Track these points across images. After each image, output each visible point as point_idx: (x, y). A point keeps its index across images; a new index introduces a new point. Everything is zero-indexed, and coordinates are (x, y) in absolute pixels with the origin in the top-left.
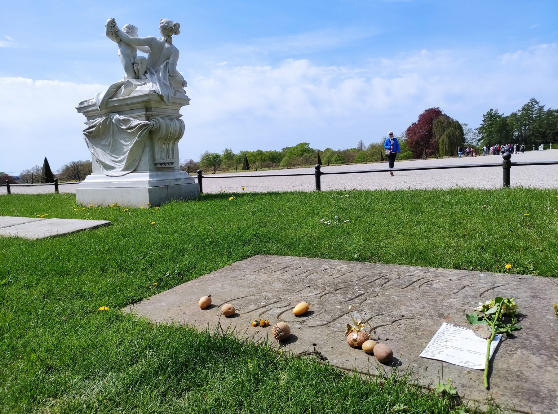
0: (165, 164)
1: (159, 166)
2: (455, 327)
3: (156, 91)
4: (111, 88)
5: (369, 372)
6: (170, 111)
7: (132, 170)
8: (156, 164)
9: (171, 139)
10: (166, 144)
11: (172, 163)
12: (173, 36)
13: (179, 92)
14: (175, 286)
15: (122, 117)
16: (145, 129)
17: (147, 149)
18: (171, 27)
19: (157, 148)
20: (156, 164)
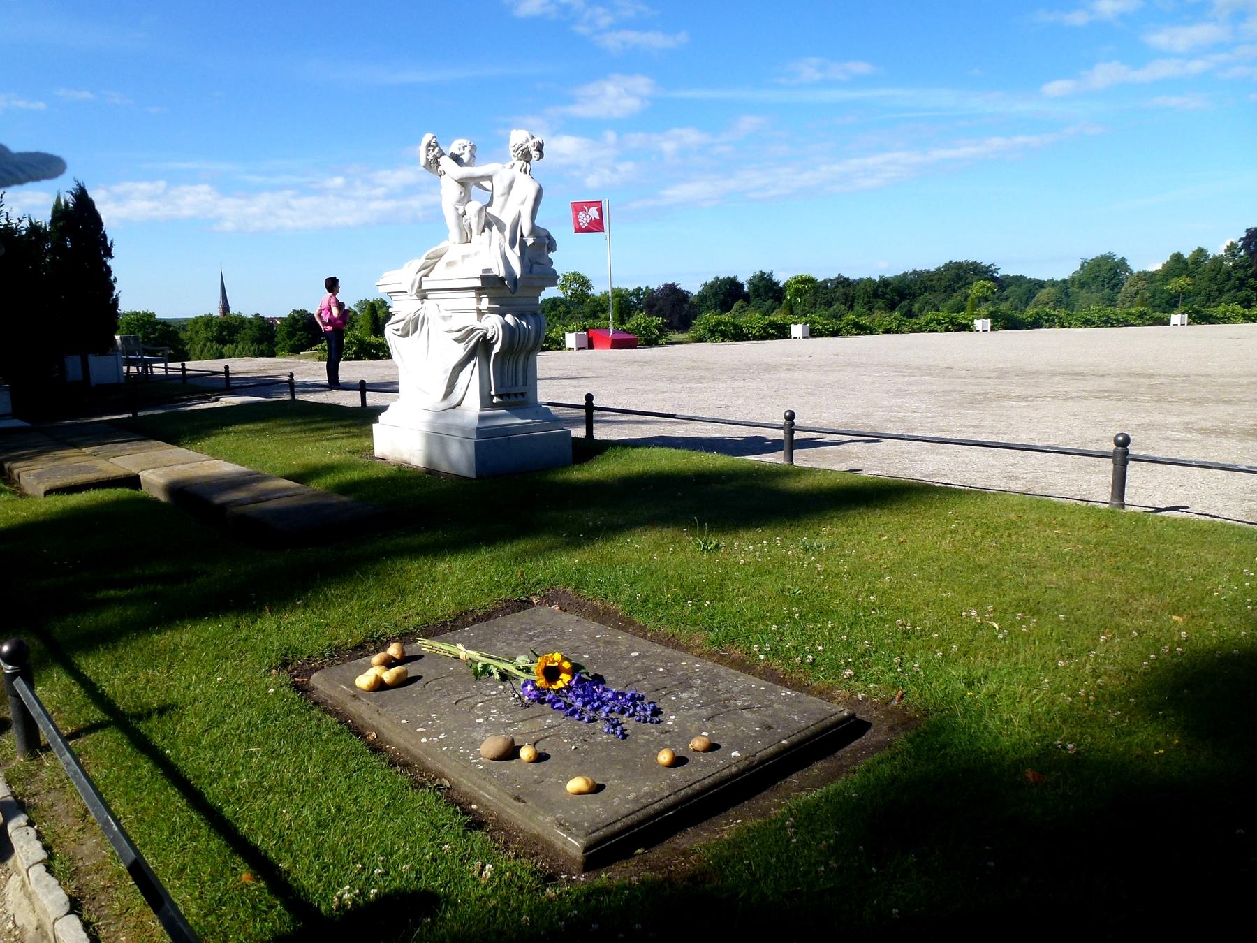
11: (523, 394)
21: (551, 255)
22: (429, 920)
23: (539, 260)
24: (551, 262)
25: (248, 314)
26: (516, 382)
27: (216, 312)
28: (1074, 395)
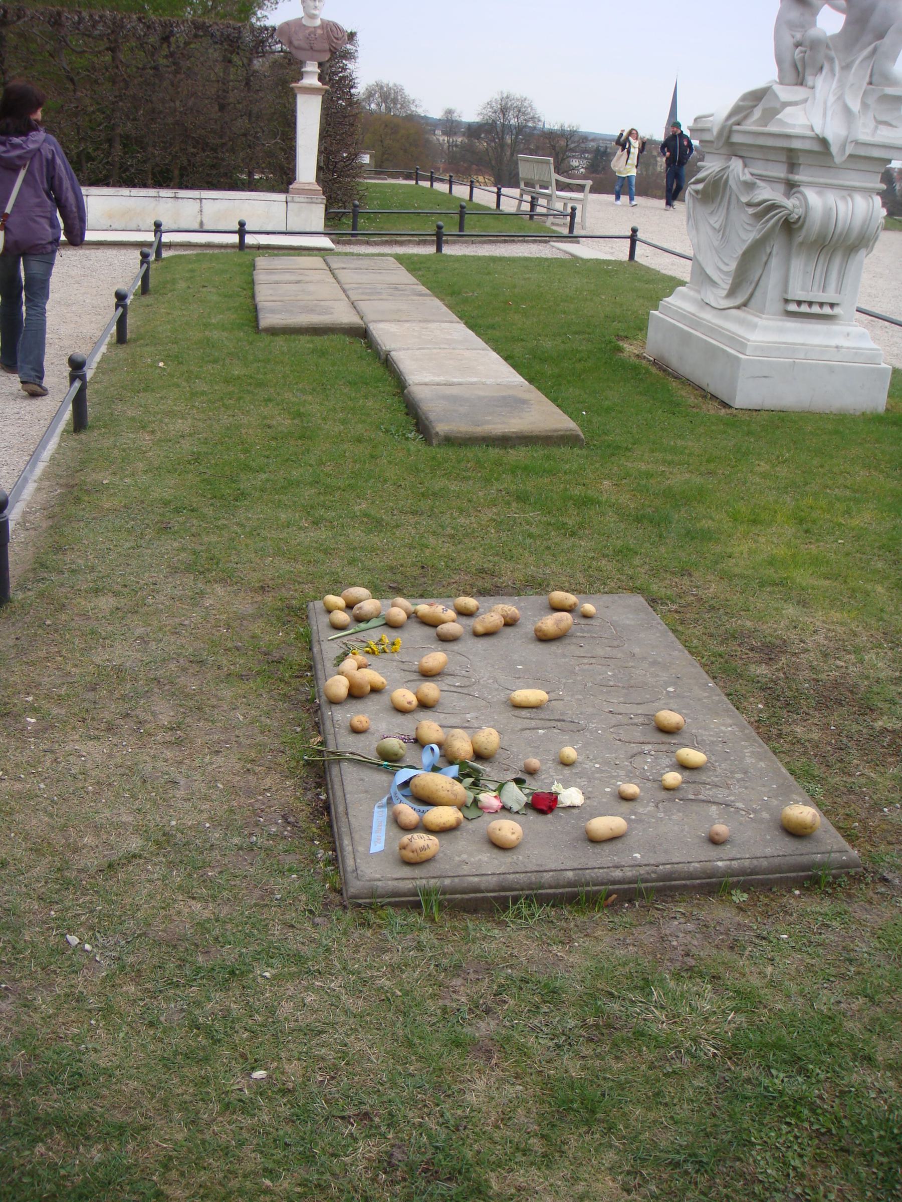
0: (810, 304)
1: (793, 307)
11: (832, 305)
20: (787, 301)
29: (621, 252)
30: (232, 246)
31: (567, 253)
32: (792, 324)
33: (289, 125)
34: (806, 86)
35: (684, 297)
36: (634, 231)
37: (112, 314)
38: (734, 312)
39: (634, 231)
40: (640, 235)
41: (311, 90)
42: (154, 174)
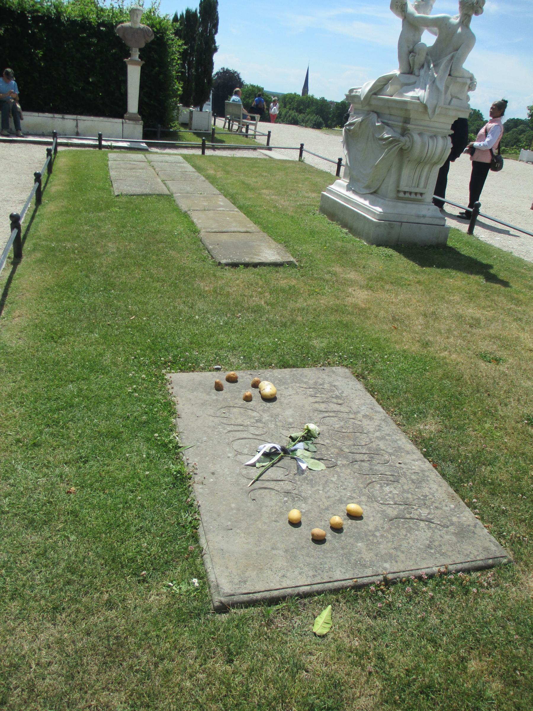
0: (410, 193)
1: (401, 195)
2: (488, 534)
3: (420, 98)
4: (379, 81)
5: (260, 480)
6: (437, 125)
7: (372, 191)
8: (398, 191)
9: (426, 163)
10: (418, 170)
11: (421, 194)
12: (474, 17)
13: (458, 98)
14: (241, 369)
15: (310, 177)
16: (391, 149)
17: (394, 170)
18: (473, 4)
19: (406, 172)
20: (398, 191)
21: (470, 93)
22: (221, 324)
23: (459, 96)
24: (468, 98)
25: (318, 96)
26: (418, 184)
27: (300, 92)
28: (398, 503)
29: (294, 155)
30: (94, 146)
31: (266, 155)
32: (400, 204)
33: (314, 125)
34: (415, 74)
35: (340, 186)
36: (302, 145)
37: (32, 185)
38: (369, 195)
39: (302, 145)
40: (304, 147)
41: (135, 63)
42: (150, 449)
